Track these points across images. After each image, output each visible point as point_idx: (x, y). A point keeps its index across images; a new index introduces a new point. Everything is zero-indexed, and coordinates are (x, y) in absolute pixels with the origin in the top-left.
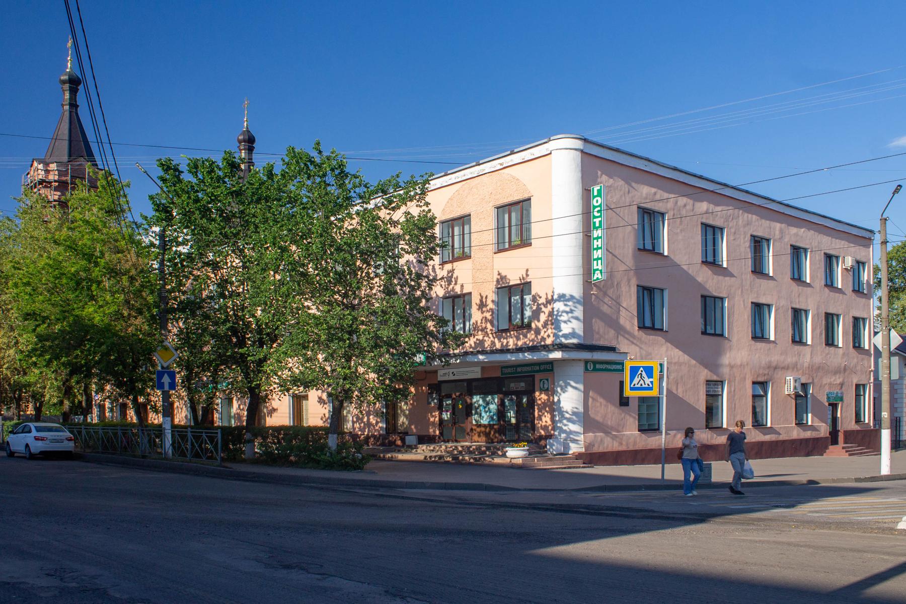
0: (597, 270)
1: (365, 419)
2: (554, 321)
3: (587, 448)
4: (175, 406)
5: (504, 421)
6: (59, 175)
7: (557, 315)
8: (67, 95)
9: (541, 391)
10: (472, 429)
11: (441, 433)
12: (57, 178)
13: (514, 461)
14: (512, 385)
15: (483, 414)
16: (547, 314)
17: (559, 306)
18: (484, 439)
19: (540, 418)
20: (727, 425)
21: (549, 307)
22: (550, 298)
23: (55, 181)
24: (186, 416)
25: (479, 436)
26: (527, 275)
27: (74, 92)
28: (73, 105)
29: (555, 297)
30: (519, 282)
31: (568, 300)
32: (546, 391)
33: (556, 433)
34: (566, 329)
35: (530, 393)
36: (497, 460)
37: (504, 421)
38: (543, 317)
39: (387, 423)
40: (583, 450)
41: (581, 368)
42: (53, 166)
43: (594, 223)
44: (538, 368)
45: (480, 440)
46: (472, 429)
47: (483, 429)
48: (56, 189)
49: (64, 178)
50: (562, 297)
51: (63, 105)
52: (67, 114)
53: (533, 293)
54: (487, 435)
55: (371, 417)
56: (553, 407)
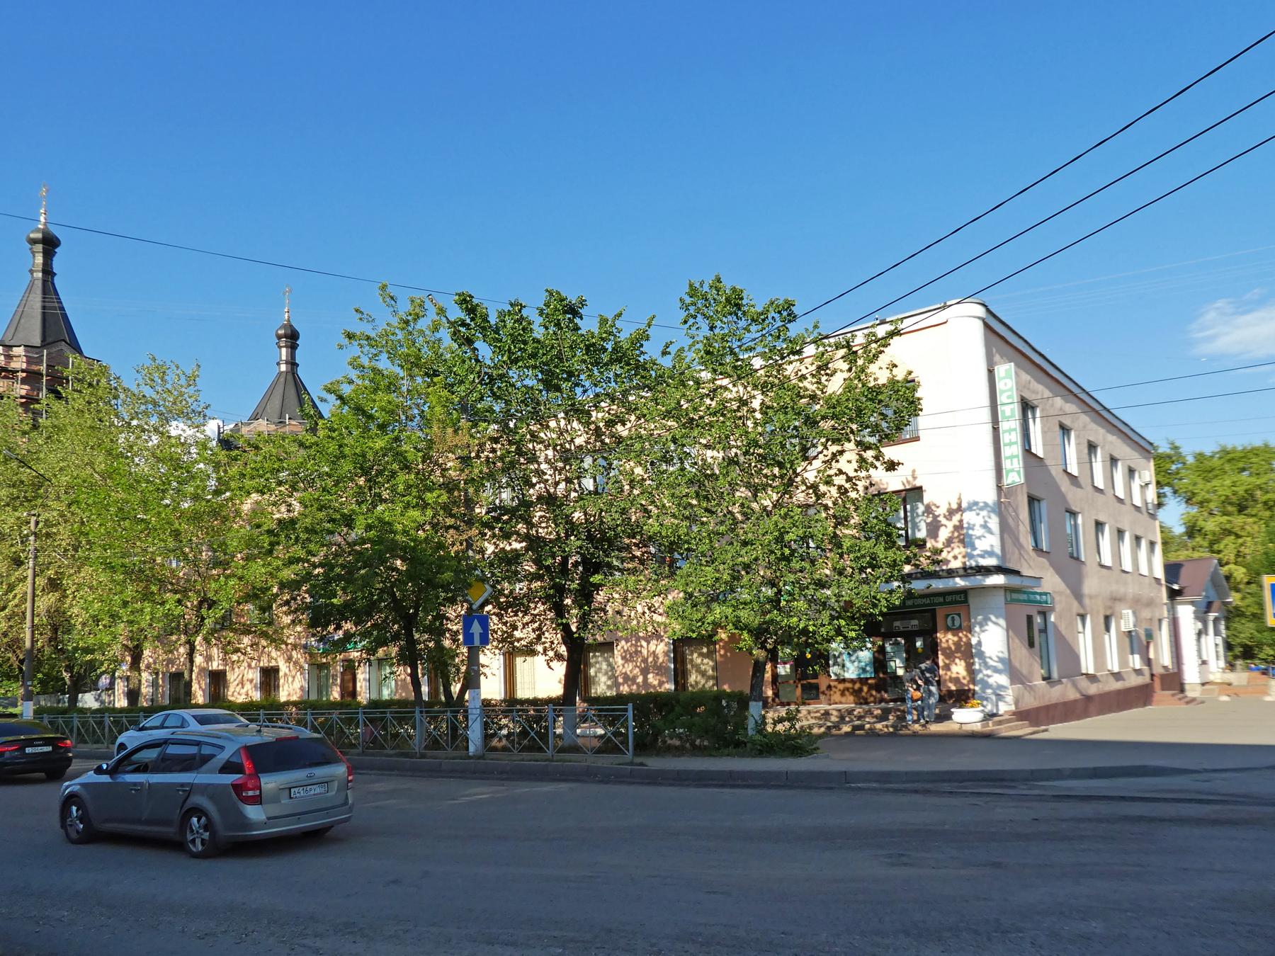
0: (1012, 470)
1: (640, 680)
2: (962, 536)
3: (1016, 703)
4: (281, 674)
5: (885, 673)
6: (28, 362)
7: (968, 528)
8: (39, 259)
9: (948, 629)
10: (829, 687)
11: (776, 695)
12: (24, 366)
13: (965, 728)
14: (897, 624)
15: (848, 664)
16: (950, 528)
17: (969, 517)
18: (851, 698)
19: (947, 668)
20: (1096, 670)
21: (956, 518)
22: (955, 506)
23: (23, 371)
24: (302, 688)
25: (843, 694)
26: (915, 478)
27: (49, 254)
28: (48, 272)
29: (964, 505)
30: (902, 488)
31: (982, 509)
32: (956, 630)
33: (977, 688)
34: (981, 545)
35: (929, 633)
36: (935, 728)
37: (885, 673)
38: (944, 534)
39: (676, 683)
40: (1013, 708)
41: (1000, 598)
42: (19, 351)
43: (1003, 412)
44: (941, 600)
45: (843, 700)
46: (829, 687)
47: (849, 685)
48: (24, 381)
49: (35, 368)
50: (973, 506)
51: (31, 272)
52: (39, 284)
53: (926, 501)
54: (857, 693)
55: (650, 676)
56: (968, 653)
